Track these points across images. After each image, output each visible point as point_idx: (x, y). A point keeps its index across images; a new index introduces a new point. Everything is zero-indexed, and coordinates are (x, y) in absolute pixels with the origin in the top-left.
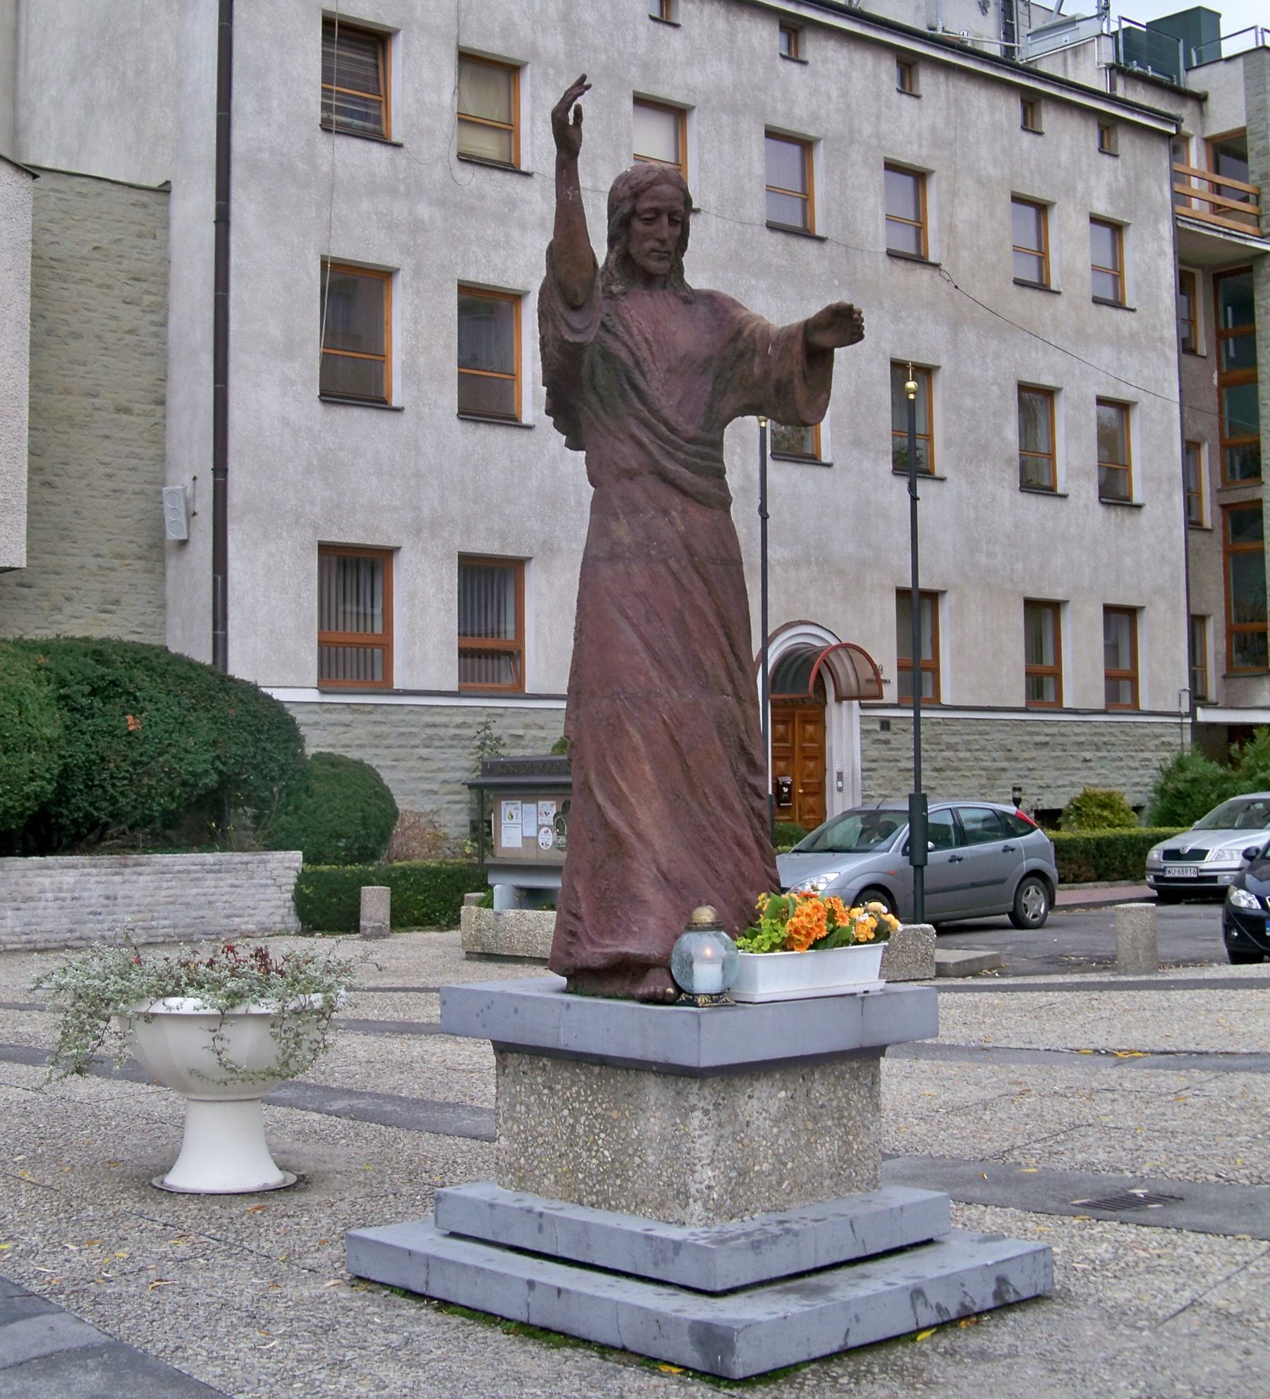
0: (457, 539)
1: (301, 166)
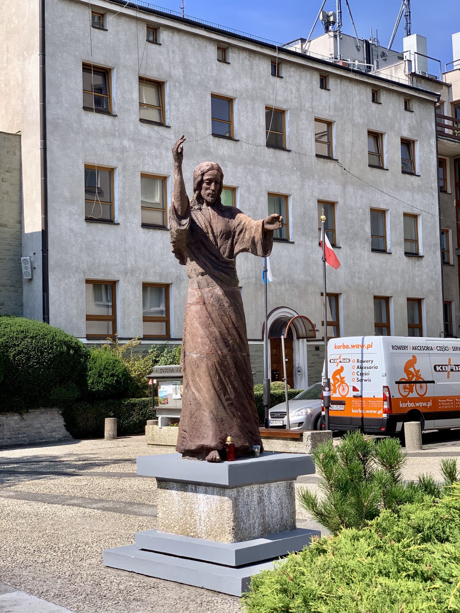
0: (142, 277)
1: (75, 125)
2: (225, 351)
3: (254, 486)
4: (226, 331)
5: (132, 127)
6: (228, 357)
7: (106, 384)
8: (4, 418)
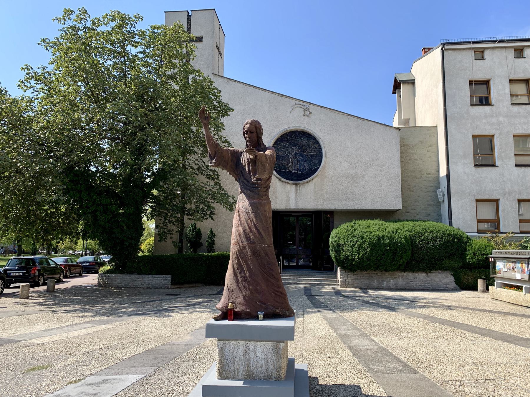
0: (517, 196)
2: (245, 243)
3: (240, 342)
4: (248, 230)
5: (505, 109)
6: (247, 248)
7: (478, 259)
8: (417, 274)
